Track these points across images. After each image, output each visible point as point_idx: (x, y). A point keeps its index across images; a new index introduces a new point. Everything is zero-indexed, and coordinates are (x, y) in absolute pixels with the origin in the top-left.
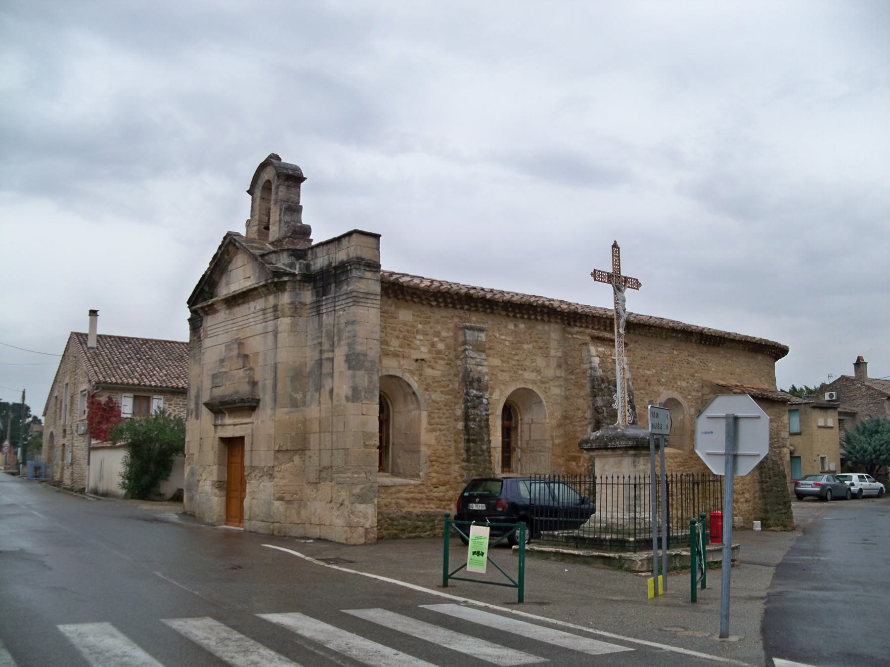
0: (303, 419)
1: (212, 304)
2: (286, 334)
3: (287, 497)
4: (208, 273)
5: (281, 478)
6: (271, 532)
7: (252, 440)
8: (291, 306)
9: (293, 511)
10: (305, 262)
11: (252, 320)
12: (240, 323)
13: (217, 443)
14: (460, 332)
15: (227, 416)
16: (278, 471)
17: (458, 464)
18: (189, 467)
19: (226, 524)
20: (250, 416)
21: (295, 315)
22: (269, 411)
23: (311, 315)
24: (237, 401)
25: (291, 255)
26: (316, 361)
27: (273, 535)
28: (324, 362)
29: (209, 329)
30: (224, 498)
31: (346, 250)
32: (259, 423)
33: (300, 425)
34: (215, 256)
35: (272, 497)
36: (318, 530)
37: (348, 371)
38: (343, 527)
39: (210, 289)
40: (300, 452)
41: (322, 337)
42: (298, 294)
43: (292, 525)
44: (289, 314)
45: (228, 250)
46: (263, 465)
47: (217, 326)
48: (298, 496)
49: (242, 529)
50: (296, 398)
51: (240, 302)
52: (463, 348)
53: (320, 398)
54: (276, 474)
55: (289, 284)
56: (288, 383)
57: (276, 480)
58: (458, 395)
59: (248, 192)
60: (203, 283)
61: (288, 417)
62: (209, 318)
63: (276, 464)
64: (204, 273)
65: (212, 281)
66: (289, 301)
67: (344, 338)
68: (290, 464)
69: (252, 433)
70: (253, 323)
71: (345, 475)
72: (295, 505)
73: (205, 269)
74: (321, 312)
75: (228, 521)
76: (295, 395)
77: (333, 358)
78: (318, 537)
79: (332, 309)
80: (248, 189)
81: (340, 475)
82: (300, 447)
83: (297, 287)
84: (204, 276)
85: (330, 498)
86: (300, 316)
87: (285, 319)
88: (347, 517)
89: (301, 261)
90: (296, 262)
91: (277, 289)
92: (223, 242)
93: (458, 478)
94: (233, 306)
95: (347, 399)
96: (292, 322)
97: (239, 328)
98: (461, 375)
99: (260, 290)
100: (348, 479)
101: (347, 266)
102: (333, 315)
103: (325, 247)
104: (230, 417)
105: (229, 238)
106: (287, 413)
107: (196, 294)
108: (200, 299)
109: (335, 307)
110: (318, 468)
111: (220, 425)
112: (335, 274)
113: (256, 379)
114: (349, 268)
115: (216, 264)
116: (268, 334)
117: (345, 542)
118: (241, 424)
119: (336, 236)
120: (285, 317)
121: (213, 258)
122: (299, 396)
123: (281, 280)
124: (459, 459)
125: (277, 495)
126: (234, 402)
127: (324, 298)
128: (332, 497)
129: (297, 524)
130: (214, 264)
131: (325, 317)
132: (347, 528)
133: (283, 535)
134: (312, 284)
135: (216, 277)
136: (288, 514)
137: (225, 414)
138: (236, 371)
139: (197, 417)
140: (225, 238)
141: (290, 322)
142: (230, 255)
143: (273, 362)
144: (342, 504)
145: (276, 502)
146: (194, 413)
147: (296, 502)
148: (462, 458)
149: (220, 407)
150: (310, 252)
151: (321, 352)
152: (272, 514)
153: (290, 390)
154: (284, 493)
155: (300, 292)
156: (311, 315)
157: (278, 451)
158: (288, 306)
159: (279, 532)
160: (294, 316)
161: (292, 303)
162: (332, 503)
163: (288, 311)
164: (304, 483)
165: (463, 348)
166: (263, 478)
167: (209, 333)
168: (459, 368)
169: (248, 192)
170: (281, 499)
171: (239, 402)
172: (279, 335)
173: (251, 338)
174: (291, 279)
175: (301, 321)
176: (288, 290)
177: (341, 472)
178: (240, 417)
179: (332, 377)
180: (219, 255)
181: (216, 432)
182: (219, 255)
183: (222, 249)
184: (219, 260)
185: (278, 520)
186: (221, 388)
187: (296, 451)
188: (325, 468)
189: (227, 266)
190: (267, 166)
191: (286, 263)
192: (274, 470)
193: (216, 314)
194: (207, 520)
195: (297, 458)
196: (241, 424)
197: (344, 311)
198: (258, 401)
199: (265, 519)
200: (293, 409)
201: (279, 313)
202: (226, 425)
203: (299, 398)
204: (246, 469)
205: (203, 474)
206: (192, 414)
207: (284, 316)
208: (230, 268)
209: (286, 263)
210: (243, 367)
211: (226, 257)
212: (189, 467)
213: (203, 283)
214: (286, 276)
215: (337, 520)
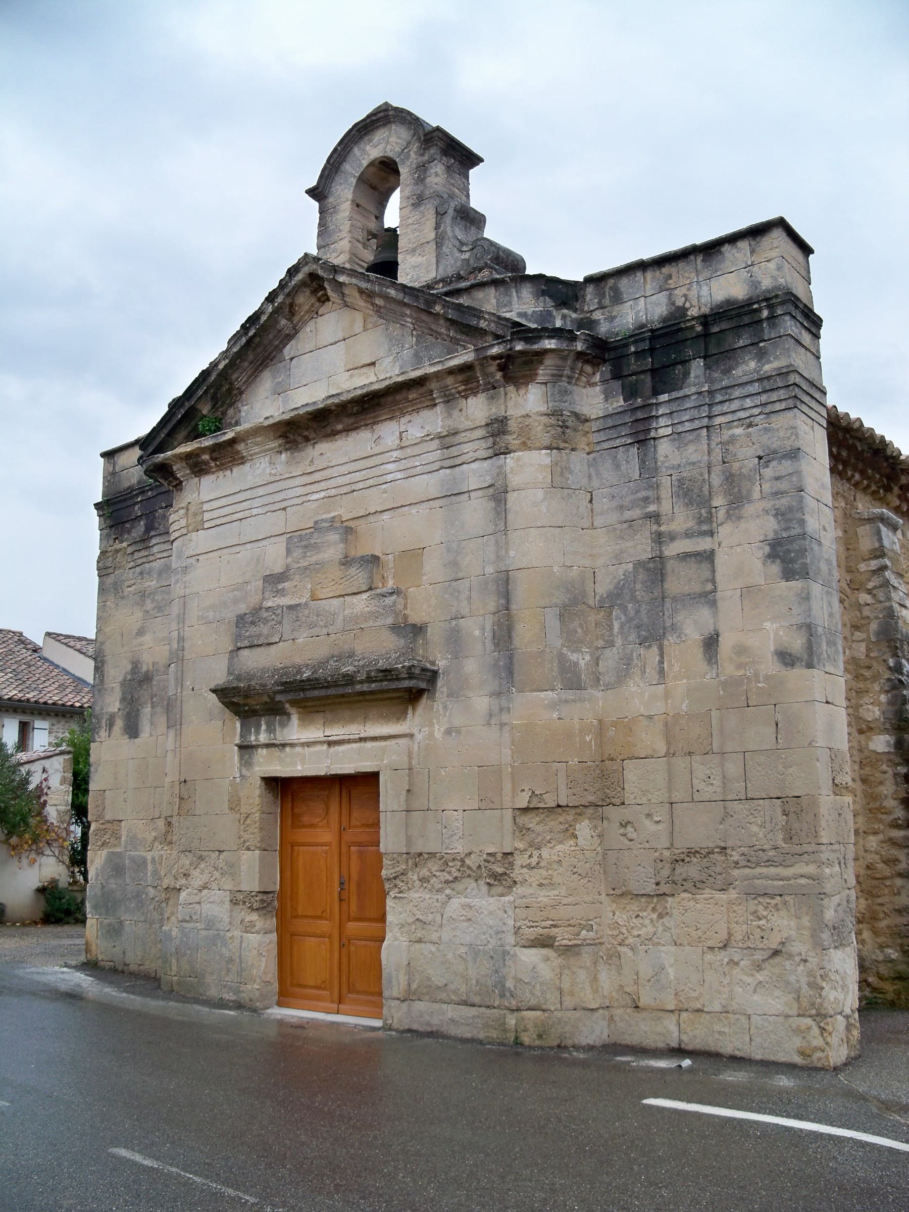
0: (595, 722)
1: (233, 442)
2: (540, 494)
3: (563, 936)
4: (221, 366)
5: (541, 885)
6: (511, 1037)
7: (410, 783)
8: (553, 421)
9: (582, 975)
10: (574, 315)
11: (391, 467)
12: (340, 481)
13: (258, 792)
14: (863, 530)
15: (295, 719)
16: (530, 867)
17: (875, 833)
18: (104, 853)
19: (280, 1004)
20: (401, 716)
21: (562, 445)
22: (481, 702)
23: (606, 445)
24: (362, 676)
25: (544, 293)
26: (639, 564)
27: (518, 1043)
28: (670, 565)
29: (206, 507)
30: (274, 937)
31: (744, 274)
32: (438, 735)
33: (588, 739)
34: (253, 319)
35: (510, 939)
36: (673, 1028)
37: (784, 584)
38: (787, 1016)
39: (214, 407)
40: (590, 811)
41: (658, 499)
42: (565, 392)
43: (578, 1014)
44: (547, 441)
45: (291, 305)
46: (459, 848)
47: (247, 495)
48: (592, 934)
49: (378, 1023)
50: (576, 664)
51: (340, 427)
52: (874, 564)
53: (661, 662)
54: (517, 873)
55: (549, 361)
56: (553, 624)
57: (519, 890)
58: (867, 674)
59: (312, 193)
60: (200, 392)
61: (555, 715)
62: (207, 481)
63: (521, 846)
64: (205, 366)
65: (226, 387)
66: (543, 408)
67: (756, 495)
68: (567, 846)
69: (410, 763)
70: (399, 475)
71: (789, 872)
72: (586, 957)
73: (213, 356)
74: (653, 434)
75: (285, 997)
76: (574, 657)
77: (712, 552)
78: (674, 1044)
79: (705, 422)
80: (313, 183)
81: (759, 870)
82: (591, 798)
83: (567, 372)
84: (205, 374)
85: (724, 936)
86: (573, 450)
87: (535, 453)
88: (805, 989)
89: (565, 311)
90: (555, 313)
91: (504, 377)
92: (282, 284)
93: (880, 866)
94: (307, 439)
95: (786, 658)
96: (554, 464)
97: (333, 492)
98: (874, 626)
99: (433, 385)
100: (803, 881)
101: (759, 310)
102: (704, 441)
103: (649, 275)
104: (306, 720)
105: (306, 270)
106: (553, 706)
107: (174, 421)
108: (181, 436)
109: (710, 417)
110: (667, 853)
111: (267, 746)
112: (706, 335)
113: (415, 618)
114: (765, 313)
115: (249, 342)
116: (458, 498)
117: (798, 1060)
118: (361, 740)
119: (699, 240)
120: (530, 449)
121: (243, 326)
122: (582, 659)
123: (535, 347)
124: (881, 821)
125: (530, 933)
126: (349, 679)
127: (664, 397)
128: (730, 934)
129: (592, 1010)
130: (244, 340)
131: (664, 448)
132: (809, 1021)
133: (555, 1043)
134: (606, 368)
135: (239, 378)
136: (566, 986)
137: (288, 715)
138: (335, 602)
139: (132, 731)
140: (292, 272)
141: (548, 461)
142: (296, 319)
143: (490, 569)
144: (776, 953)
145: (525, 951)
146: (119, 724)
147: (587, 949)
148: (888, 819)
149: (278, 698)
150: (590, 289)
151: (659, 538)
152: (510, 984)
153: (558, 643)
154: (555, 926)
155: (569, 387)
156: (606, 445)
157: (526, 810)
158: (545, 419)
159: (540, 1036)
160: (558, 449)
161: (555, 413)
162: (730, 951)
163: (540, 431)
164: (603, 897)
165: (874, 564)
166: (459, 886)
167: (207, 516)
168: (866, 612)
169: (312, 193)
170: (544, 943)
171: (369, 679)
172: (512, 497)
173: (386, 516)
174: (564, 346)
175: (578, 461)
176: (540, 379)
177: (770, 862)
178: (352, 720)
179: (713, 604)
180: (264, 318)
181: (246, 763)
182: (264, 318)
183: (280, 299)
184: (264, 328)
185: (533, 1002)
186: (273, 648)
187: (580, 809)
188: (692, 853)
189: (279, 349)
190: (377, 128)
191: (530, 312)
192: (511, 864)
193: (236, 470)
194: (213, 992)
195: (584, 828)
196: (361, 740)
197: (750, 425)
198: (433, 676)
199: (476, 1000)
200: (570, 695)
201: (512, 440)
202: (292, 745)
203: (582, 663)
204: (385, 861)
205: (195, 873)
206: (111, 725)
207: (525, 446)
208: (288, 351)
209: (530, 312)
210: (370, 589)
211: (283, 322)
212: (104, 853)
213: (200, 392)
214: (550, 337)
215: (756, 997)
